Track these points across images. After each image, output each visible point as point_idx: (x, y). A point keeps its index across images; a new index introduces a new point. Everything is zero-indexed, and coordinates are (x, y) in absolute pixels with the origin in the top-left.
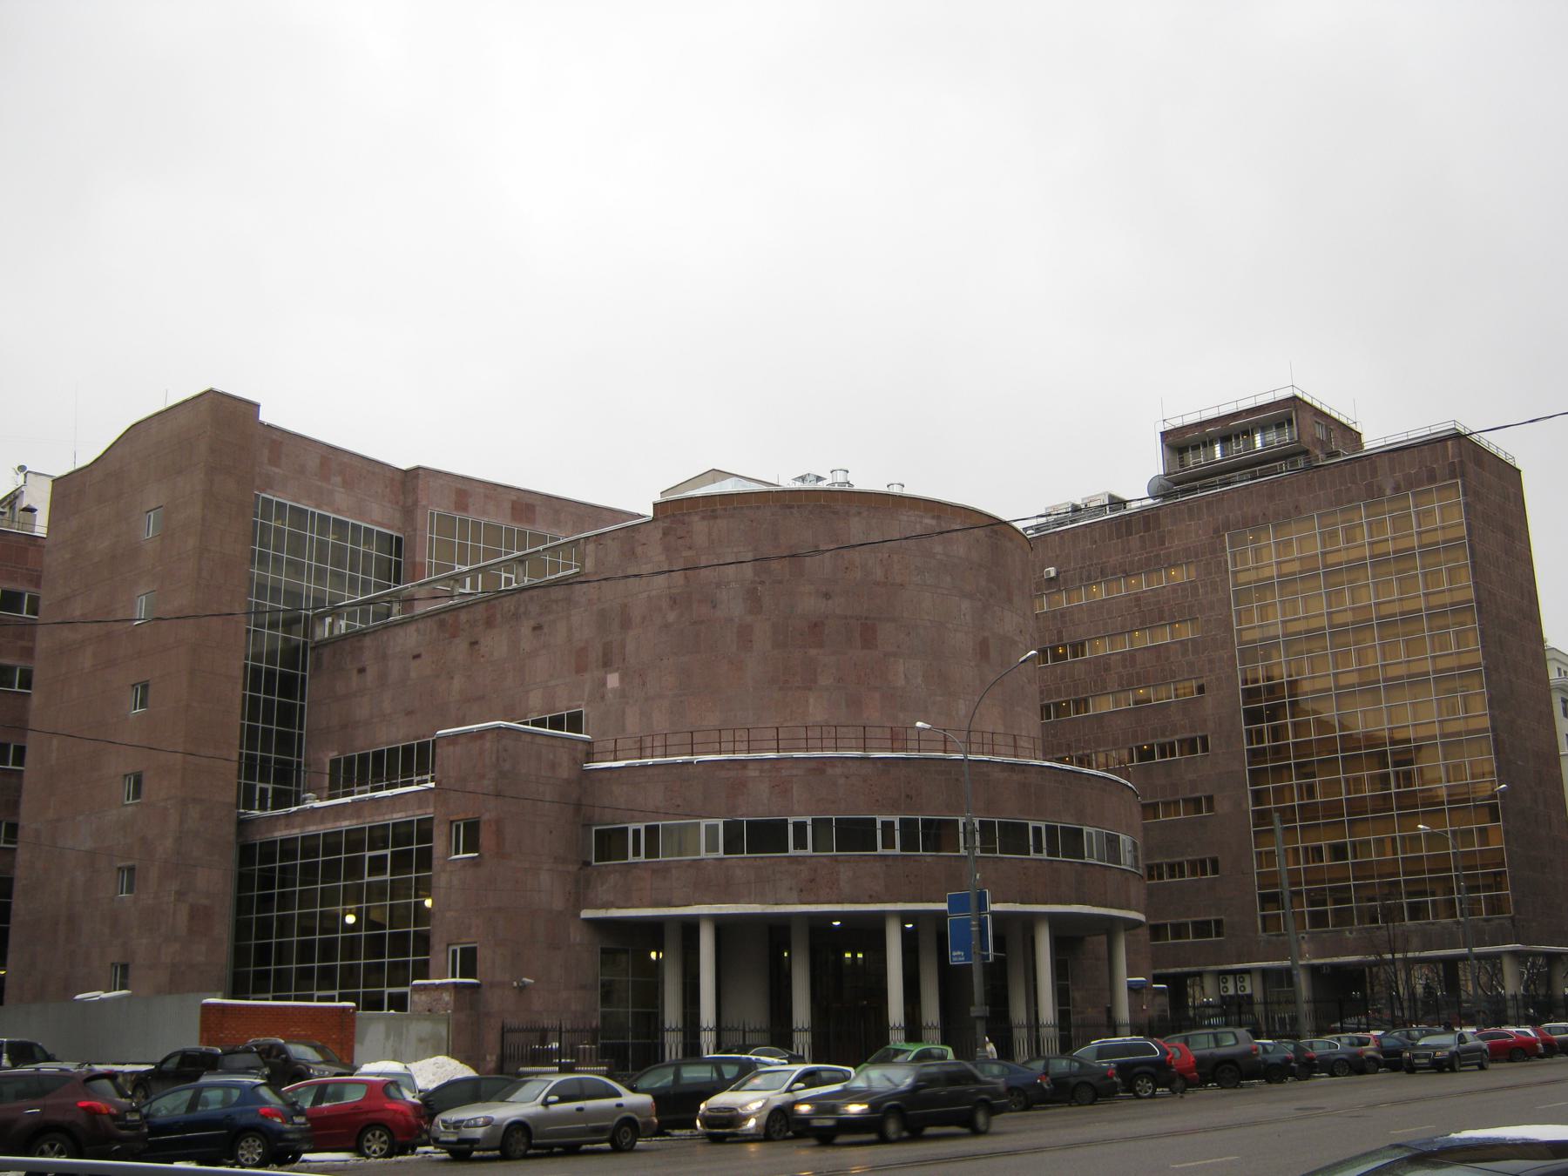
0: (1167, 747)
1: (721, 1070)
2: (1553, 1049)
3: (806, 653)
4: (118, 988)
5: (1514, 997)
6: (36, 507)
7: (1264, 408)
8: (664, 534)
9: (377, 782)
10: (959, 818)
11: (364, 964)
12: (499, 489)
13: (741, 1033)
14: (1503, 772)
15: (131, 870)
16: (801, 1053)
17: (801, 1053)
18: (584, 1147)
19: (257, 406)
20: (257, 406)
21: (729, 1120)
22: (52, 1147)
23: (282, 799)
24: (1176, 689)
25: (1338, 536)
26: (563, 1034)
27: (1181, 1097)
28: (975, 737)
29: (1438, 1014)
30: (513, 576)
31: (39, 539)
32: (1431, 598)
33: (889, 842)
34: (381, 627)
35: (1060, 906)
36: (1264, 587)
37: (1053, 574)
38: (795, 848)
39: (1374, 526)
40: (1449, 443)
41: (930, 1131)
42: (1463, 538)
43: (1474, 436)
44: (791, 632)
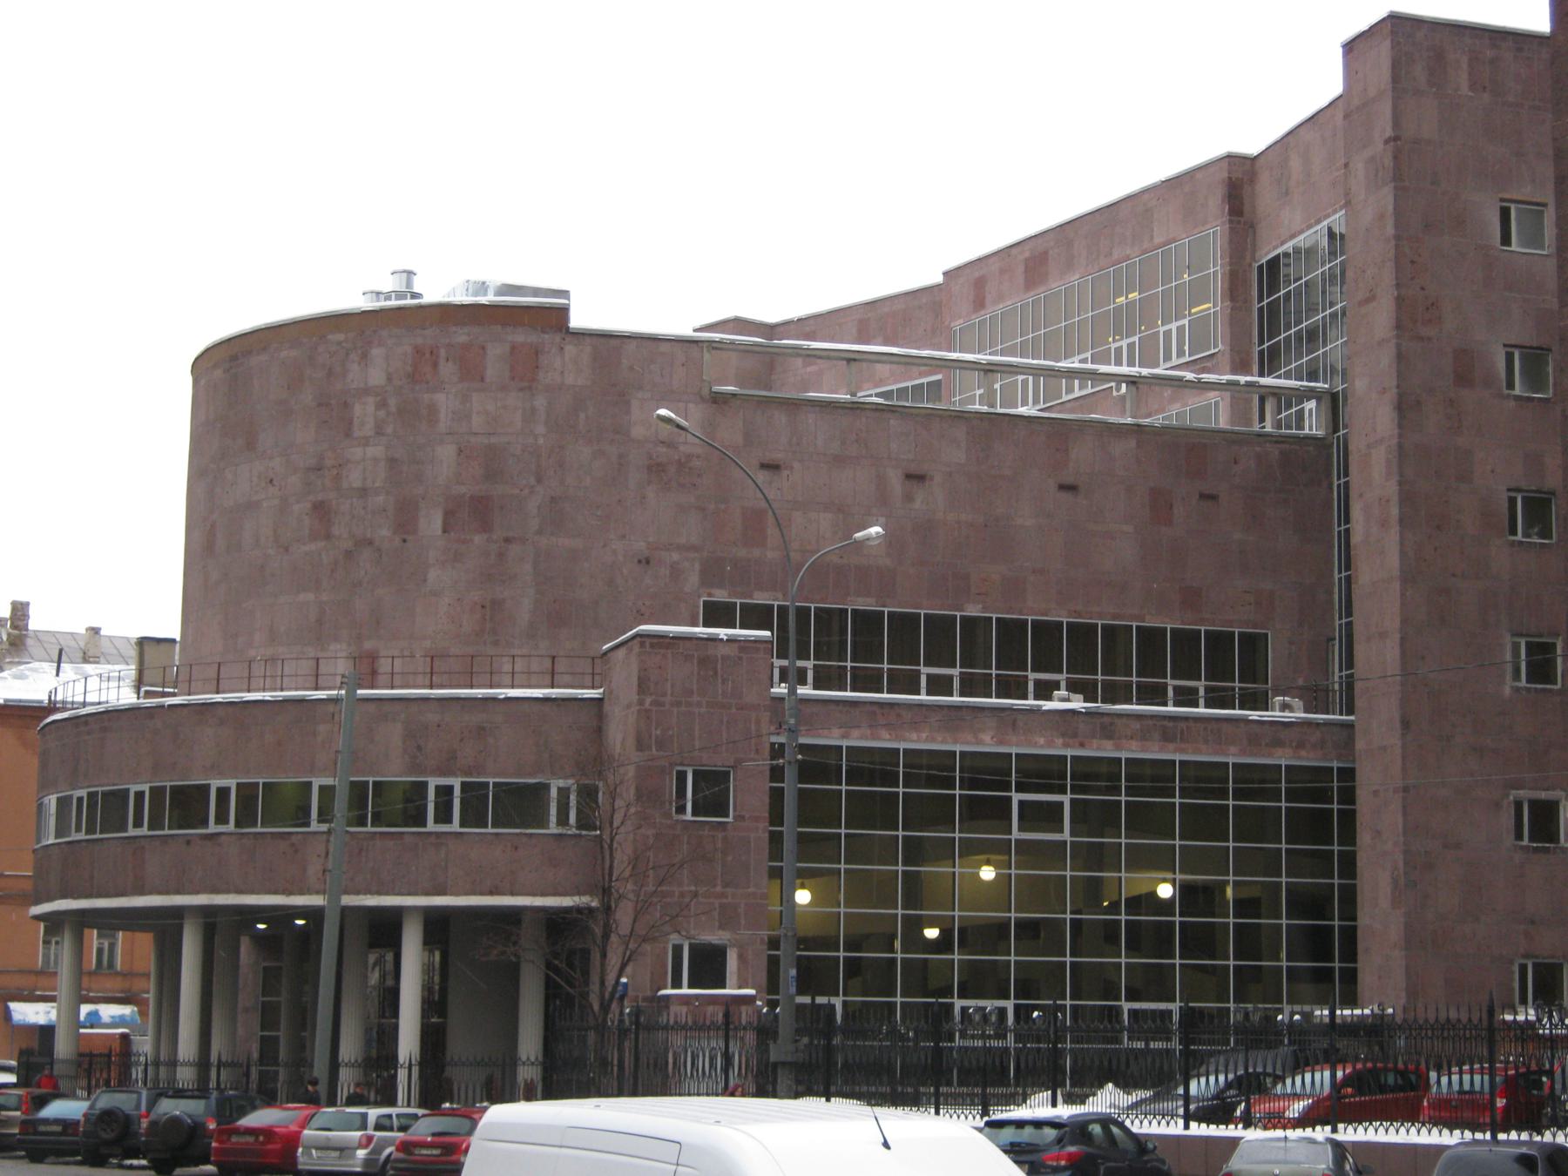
11: (1333, 969)
12: (664, 347)
29: (450, 656)
33: (444, 815)
38: (436, 822)
42: (1545, 205)
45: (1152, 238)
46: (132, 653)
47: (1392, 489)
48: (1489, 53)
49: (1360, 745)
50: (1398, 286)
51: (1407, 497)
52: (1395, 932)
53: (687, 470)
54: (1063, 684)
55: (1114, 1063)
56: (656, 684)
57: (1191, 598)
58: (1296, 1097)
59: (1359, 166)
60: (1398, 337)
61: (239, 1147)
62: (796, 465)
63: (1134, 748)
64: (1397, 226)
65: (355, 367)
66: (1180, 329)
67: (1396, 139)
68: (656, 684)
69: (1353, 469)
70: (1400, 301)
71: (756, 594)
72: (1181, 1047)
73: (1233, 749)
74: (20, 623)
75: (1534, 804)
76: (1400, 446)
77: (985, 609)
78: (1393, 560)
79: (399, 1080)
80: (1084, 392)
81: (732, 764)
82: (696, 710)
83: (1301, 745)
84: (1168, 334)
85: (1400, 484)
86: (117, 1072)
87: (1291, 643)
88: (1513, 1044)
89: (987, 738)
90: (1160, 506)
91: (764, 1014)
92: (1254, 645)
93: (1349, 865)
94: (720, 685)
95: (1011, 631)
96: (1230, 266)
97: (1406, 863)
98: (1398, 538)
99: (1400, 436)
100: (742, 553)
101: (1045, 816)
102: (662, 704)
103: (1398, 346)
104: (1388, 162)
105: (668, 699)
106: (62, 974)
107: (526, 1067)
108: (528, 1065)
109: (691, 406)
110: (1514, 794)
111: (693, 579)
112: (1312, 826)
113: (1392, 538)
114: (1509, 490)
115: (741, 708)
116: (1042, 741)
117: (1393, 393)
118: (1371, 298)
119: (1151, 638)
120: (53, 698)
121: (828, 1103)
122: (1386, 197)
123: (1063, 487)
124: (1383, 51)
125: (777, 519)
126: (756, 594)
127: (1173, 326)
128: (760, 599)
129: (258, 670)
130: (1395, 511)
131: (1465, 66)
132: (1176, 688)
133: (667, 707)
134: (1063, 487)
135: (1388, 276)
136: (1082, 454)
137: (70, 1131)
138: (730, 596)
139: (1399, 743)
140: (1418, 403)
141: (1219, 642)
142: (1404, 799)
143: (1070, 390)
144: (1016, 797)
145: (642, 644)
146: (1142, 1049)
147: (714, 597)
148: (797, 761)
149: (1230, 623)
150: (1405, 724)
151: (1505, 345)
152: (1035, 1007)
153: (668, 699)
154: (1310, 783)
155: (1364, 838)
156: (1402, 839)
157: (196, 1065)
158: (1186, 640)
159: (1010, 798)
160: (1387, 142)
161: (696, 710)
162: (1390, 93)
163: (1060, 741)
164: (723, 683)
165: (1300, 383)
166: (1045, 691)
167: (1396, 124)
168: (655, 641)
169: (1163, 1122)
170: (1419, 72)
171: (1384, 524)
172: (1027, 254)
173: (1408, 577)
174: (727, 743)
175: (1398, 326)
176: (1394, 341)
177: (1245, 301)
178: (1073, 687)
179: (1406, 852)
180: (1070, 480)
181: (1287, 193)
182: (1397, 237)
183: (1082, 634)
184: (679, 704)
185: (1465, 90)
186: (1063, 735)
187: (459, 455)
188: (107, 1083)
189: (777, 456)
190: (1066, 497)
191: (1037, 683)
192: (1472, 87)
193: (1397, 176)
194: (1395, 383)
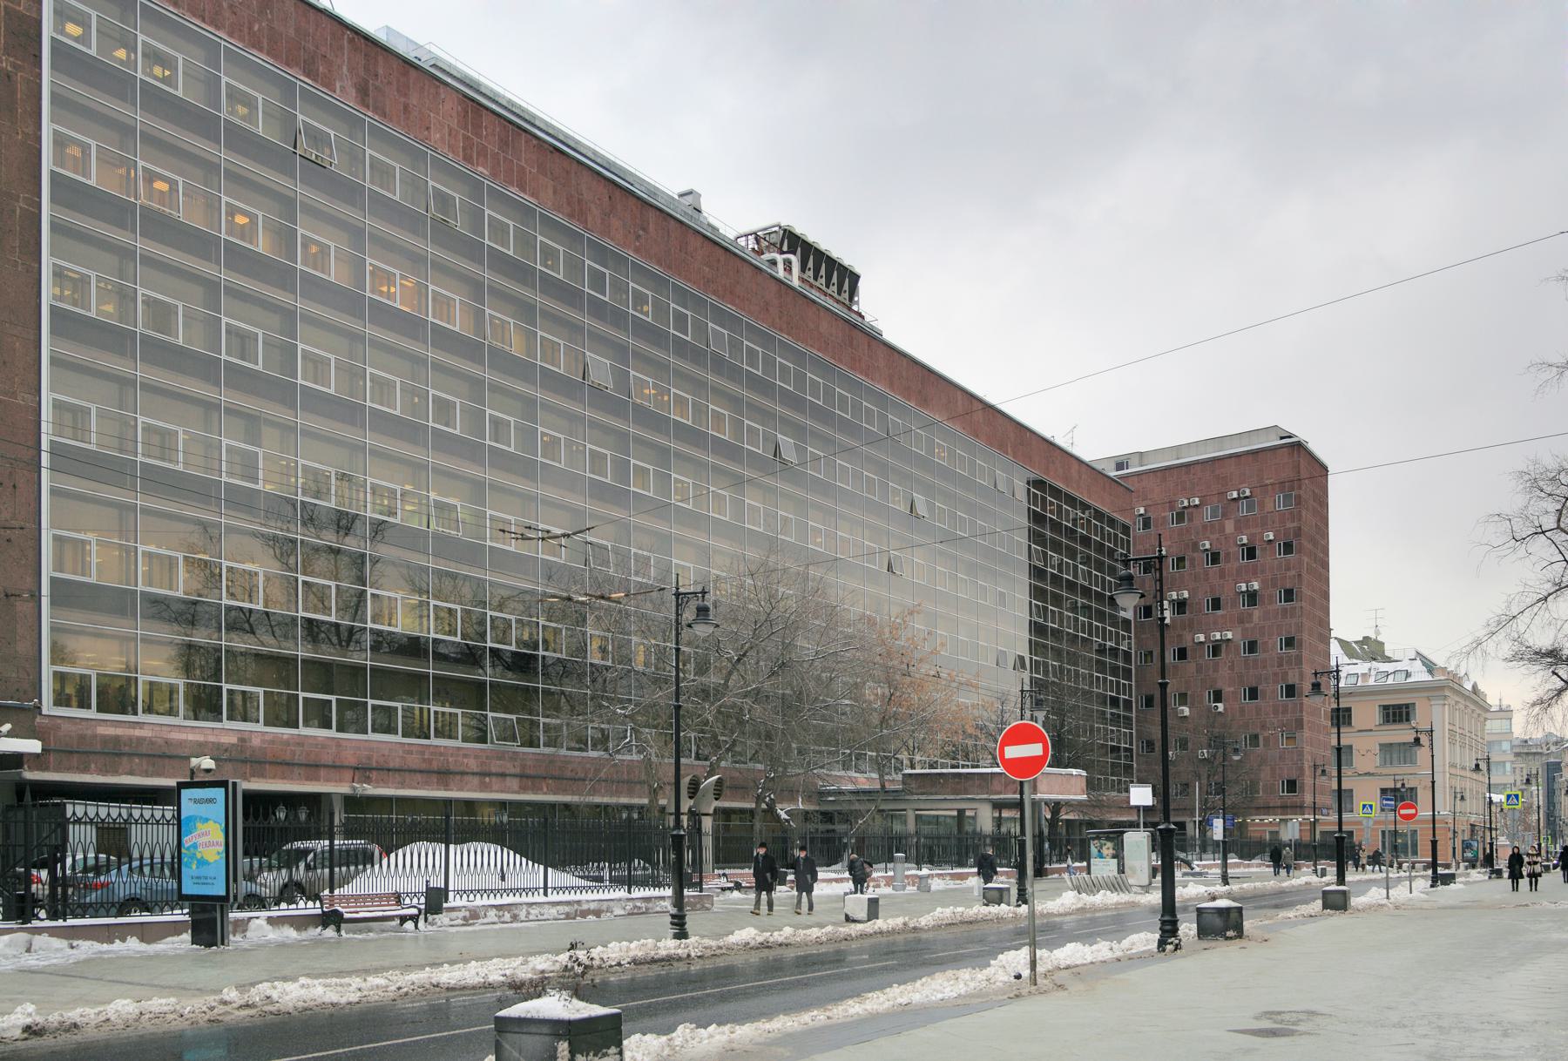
0: (28, 788)
1: (187, 895)
2: (1561, 946)
3: (1143, 596)
4: (53, 354)
5: (1091, 785)
7: (1071, 806)
8: (1433, 881)
9: (231, 703)
10: (180, 430)
13: (549, 885)
14: (816, 873)
15: (28, 950)
16: (955, 813)
17: (955, 813)
18: (1488, 851)
19: (700, 195)
20: (700, 195)
21: (808, 798)
22: (108, 911)
23: (846, 767)
24: (529, 913)
25: (244, 477)
26: (542, 886)
27: (1336, 902)
28: (345, 635)
29: (1388, 889)
30: (590, 726)
31: (132, 305)
32: (1192, 824)
34: (426, 722)
35: (133, 778)
36: (1225, 865)
37: (1271, 537)
38: (331, 701)
39: (133, 668)
40: (1018, 796)
41: (76, 276)
43: (29, 444)
46: (1229, 880)
53: (145, 767)
55: (157, 855)
58: (73, 894)
61: (884, 940)
63: (487, 810)
65: (264, 630)
72: (43, 914)
74: (1067, 620)
79: (133, 841)
80: (367, 265)
86: (166, 1009)
88: (1402, 755)
91: (15, 871)
94: (345, 789)
96: (992, 877)
106: (1249, 866)
108: (85, 823)
110: (1383, 827)
114: (758, 914)
120: (1388, 756)
125: (307, 765)
129: (935, 820)
132: (374, 708)
137: (349, 714)
146: (440, 889)
147: (73, 663)
148: (197, 867)
152: (245, 213)
157: (1034, 945)
165: (288, 732)
166: (622, 669)
169: (498, 895)
174: (584, 780)
187: (313, 549)
188: (61, 298)
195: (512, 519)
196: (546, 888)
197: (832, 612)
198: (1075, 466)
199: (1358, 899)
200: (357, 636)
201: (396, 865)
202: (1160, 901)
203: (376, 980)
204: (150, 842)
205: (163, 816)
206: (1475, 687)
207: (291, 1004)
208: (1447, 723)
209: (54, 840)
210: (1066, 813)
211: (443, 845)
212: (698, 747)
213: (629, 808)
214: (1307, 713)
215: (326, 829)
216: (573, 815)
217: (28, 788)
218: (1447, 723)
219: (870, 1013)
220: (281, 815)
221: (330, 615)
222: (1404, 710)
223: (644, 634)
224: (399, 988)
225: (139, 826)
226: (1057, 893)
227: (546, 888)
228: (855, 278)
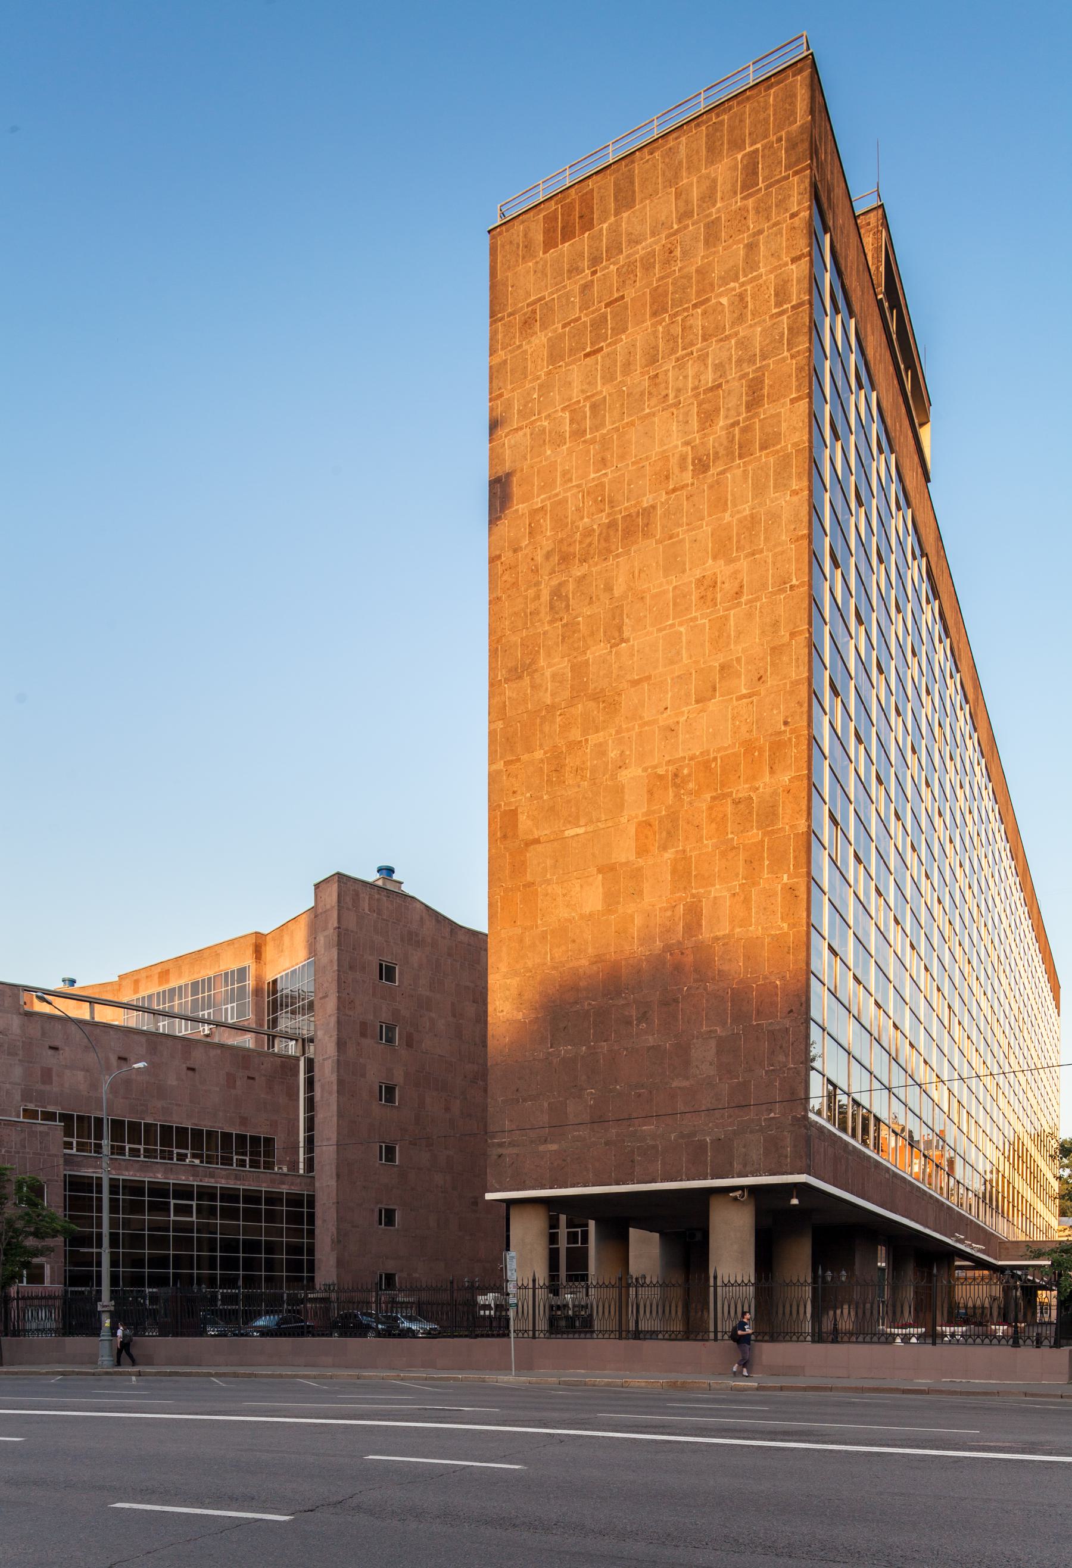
0: (551, 1246)
6: (401, 880)
10: (718, 1028)
11: (144, 1286)
13: (719, 1329)
33: (683, 468)
44: (202, 1162)
45: (219, 967)
47: (334, 1078)
48: (376, 896)
49: (317, 1184)
50: (338, 992)
51: (340, 1082)
52: (333, 1261)
54: (189, 1155)
56: (7, 1142)
57: (244, 1121)
59: (321, 939)
60: (338, 1013)
62: (67, 1049)
64: (339, 966)
66: (232, 1008)
67: (339, 928)
68: (7, 1142)
69: (316, 1069)
70: (339, 997)
71: (48, 1107)
73: (264, 1185)
75: (386, 1210)
76: (338, 1060)
77: (155, 1120)
78: (334, 1107)
79: (810, 1322)
81: (325, 1062)
82: (28, 1156)
83: (292, 1184)
84: (226, 1009)
85: (338, 1076)
87: (284, 1142)
89: (159, 1176)
90: (231, 1080)
92: (269, 1142)
93: (311, 1233)
95: (166, 1130)
97: (338, 1233)
98: (336, 1099)
99: (338, 1056)
100: (42, 1087)
101: (186, 1210)
102: (11, 1152)
103: (338, 1017)
104: (336, 938)
105: (13, 1150)
107: (741, 1288)
109: (14, 1016)
110: (379, 1206)
111: (18, 1097)
112: (295, 1218)
113: (334, 1098)
115: (49, 1155)
116: (184, 1178)
117: (335, 1038)
118: (326, 996)
119: (227, 1136)
121: (395, 871)
122: (335, 952)
123: (189, 1069)
124: (334, 888)
126: (48, 1107)
127: (229, 1006)
128: (50, 1109)
130: (335, 1087)
131: (367, 900)
133: (13, 1154)
134: (189, 1069)
135: (334, 987)
136: (198, 1056)
138: (36, 1107)
139: (335, 1184)
140: (346, 1042)
141: (255, 1140)
142: (337, 1207)
143: (209, 1014)
144: (173, 1202)
145: (338, 877)
149: (259, 1133)
150: (338, 1176)
151: (380, 1022)
153: (13, 1150)
154: (295, 1200)
155: (318, 1222)
156: (336, 1223)
158: (242, 1138)
159: (170, 1202)
160: (335, 929)
161: (28, 1156)
162: (336, 908)
163: (191, 1178)
164: (40, 1143)
167: (339, 922)
168: (6, 1122)
170: (348, 899)
171: (330, 1093)
172: (159, 970)
173: (340, 1115)
175: (338, 1009)
176: (336, 1015)
177: (262, 997)
178: (194, 1156)
179: (338, 1229)
180: (192, 1066)
181: (282, 951)
182: (339, 971)
183: (197, 1133)
184: (18, 1153)
185: (367, 911)
186: (193, 1176)
189: (56, 1044)
190: (190, 1073)
191: (178, 1154)
192: (370, 910)
193: (339, 944)
194: (336, 1033)
195: (267, 1000)
196: (534, 1331)
197: (1065, 1140)
198: (73, 1028)
199: (884, 1252)
200: (570, 762)
201: (645, 1307)
202: (511, 1210)
203: (602, 1378)
204: (981, 1296)
205: (523, 1334)
206: (111, 1301)
207: (537, 997)
208: (217, 1166)
209: (509, 691)
210: (673, 791)
211: (640, 1329)
212: (801, 312)
213: (114, 1263)
214: (805, 325)
215: (373, 1299)
216: (502, 447)
217: (551, 1246)
218: (217, 1166)
219: (315, 915)
220: (590, 995)
221: (72, 1149)
222: (154, 1154)
223: (623, 419)
224: (781, 294)
225: (796, 1287)
226: (16, 1186)
227: (534, 1331)
228: (317, 886)
